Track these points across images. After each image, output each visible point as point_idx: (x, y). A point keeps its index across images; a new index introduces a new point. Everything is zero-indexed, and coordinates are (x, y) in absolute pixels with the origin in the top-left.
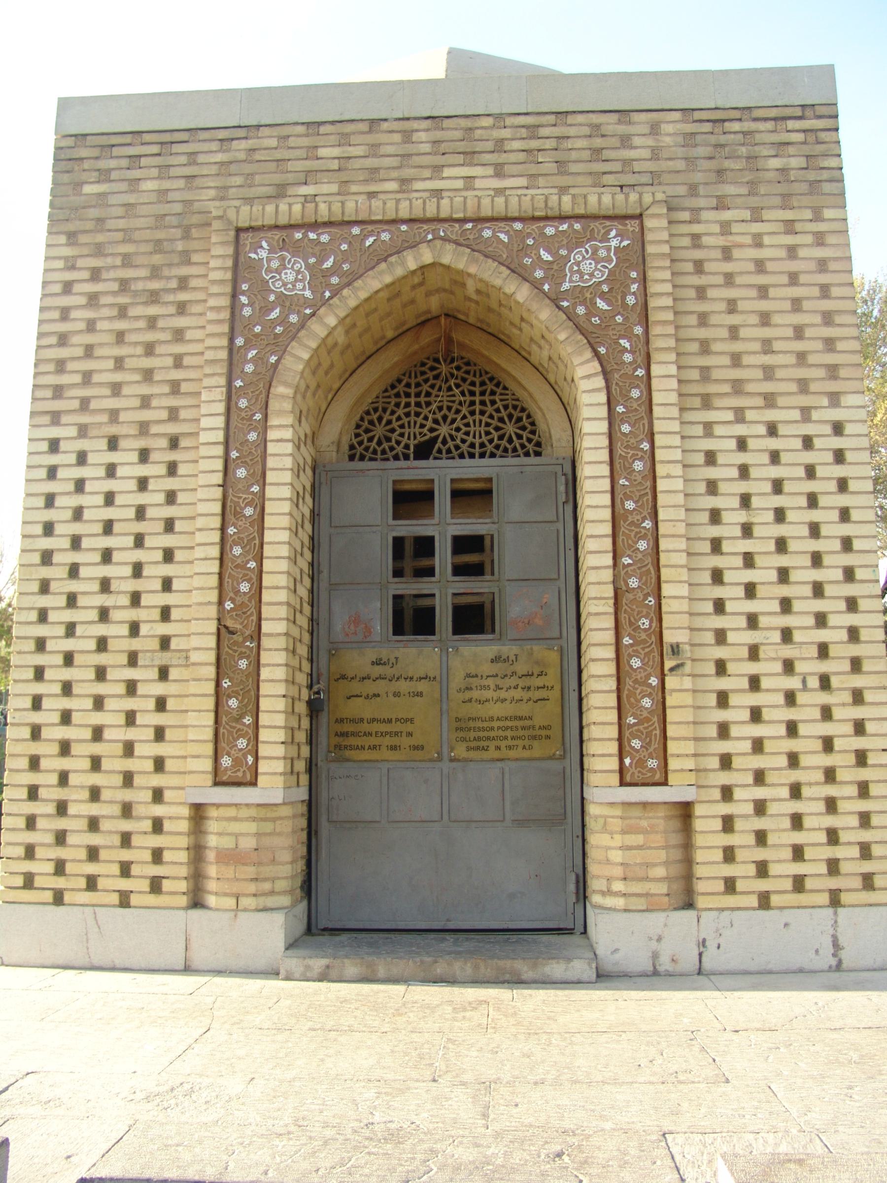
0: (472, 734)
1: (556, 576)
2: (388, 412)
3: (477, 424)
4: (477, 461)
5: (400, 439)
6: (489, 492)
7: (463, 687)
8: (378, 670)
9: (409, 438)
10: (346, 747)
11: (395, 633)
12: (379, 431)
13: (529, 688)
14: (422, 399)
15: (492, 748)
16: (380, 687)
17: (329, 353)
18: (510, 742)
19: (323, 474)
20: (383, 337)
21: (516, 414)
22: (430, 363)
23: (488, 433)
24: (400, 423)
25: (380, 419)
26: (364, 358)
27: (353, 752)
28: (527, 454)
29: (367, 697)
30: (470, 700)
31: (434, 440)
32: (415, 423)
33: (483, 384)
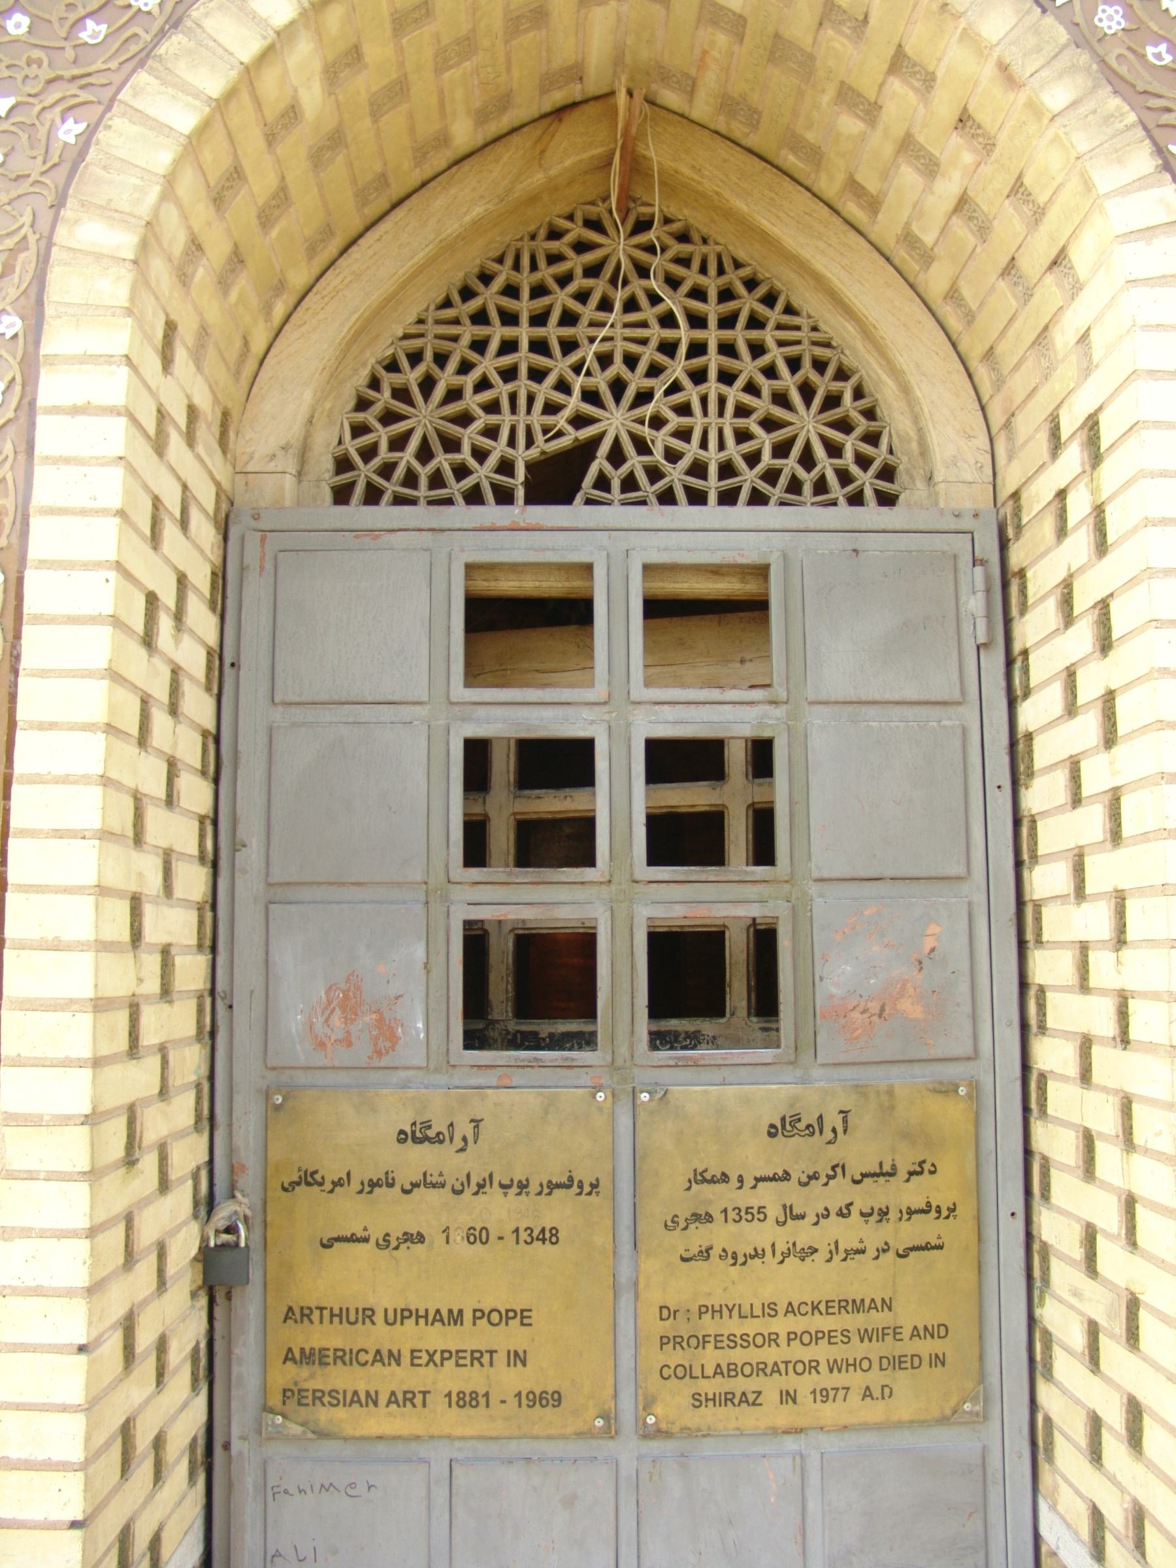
0: (710, 1357)
1: (960, 870)
2: (452, 365)
3: (713, 406)
4: (712, 513)
5: (486, 442)
6: (757, 607)
7: (684, 1214)
8: (417, 1160)
9: (512, 443)
10: (318, 1397)
11: (473, 1040)
12: (425, 418)
13: (884, 1213)
14: (553, 332)
15: (771, 1396)
16: (425, 1212)
17: (271, 139)
18: (826, 1380)
19: (253, 540)
20: (443, 139)
21: (824, 385)
22: (577, 231)
23: (743, 436)
24: (486, 396)
25: (428, 385)
26: (383, 204)
27: (341, 1413)
28: (856, 499)
29: (385, 1243)
30: (705, 1254)
31: (587, 449)
32: (531, 399)
33: (726, 295)
